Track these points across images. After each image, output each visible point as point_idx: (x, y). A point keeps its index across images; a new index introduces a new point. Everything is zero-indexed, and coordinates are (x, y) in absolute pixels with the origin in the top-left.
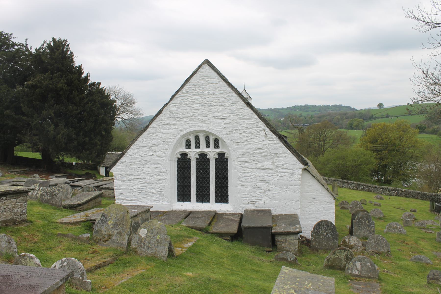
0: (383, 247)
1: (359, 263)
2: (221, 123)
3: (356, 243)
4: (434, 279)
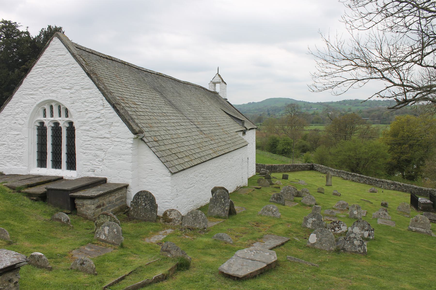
0: (200, 223)
2: (67, 93)
3: (175, 217)
4: (166, 251)
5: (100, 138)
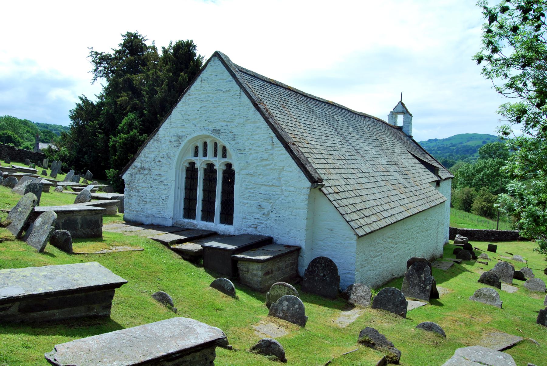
1: (287, 303)
5: (266, 185)
